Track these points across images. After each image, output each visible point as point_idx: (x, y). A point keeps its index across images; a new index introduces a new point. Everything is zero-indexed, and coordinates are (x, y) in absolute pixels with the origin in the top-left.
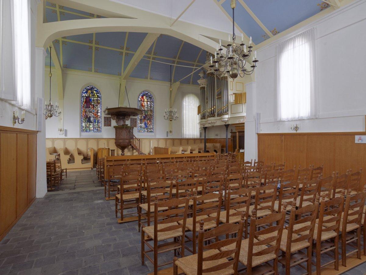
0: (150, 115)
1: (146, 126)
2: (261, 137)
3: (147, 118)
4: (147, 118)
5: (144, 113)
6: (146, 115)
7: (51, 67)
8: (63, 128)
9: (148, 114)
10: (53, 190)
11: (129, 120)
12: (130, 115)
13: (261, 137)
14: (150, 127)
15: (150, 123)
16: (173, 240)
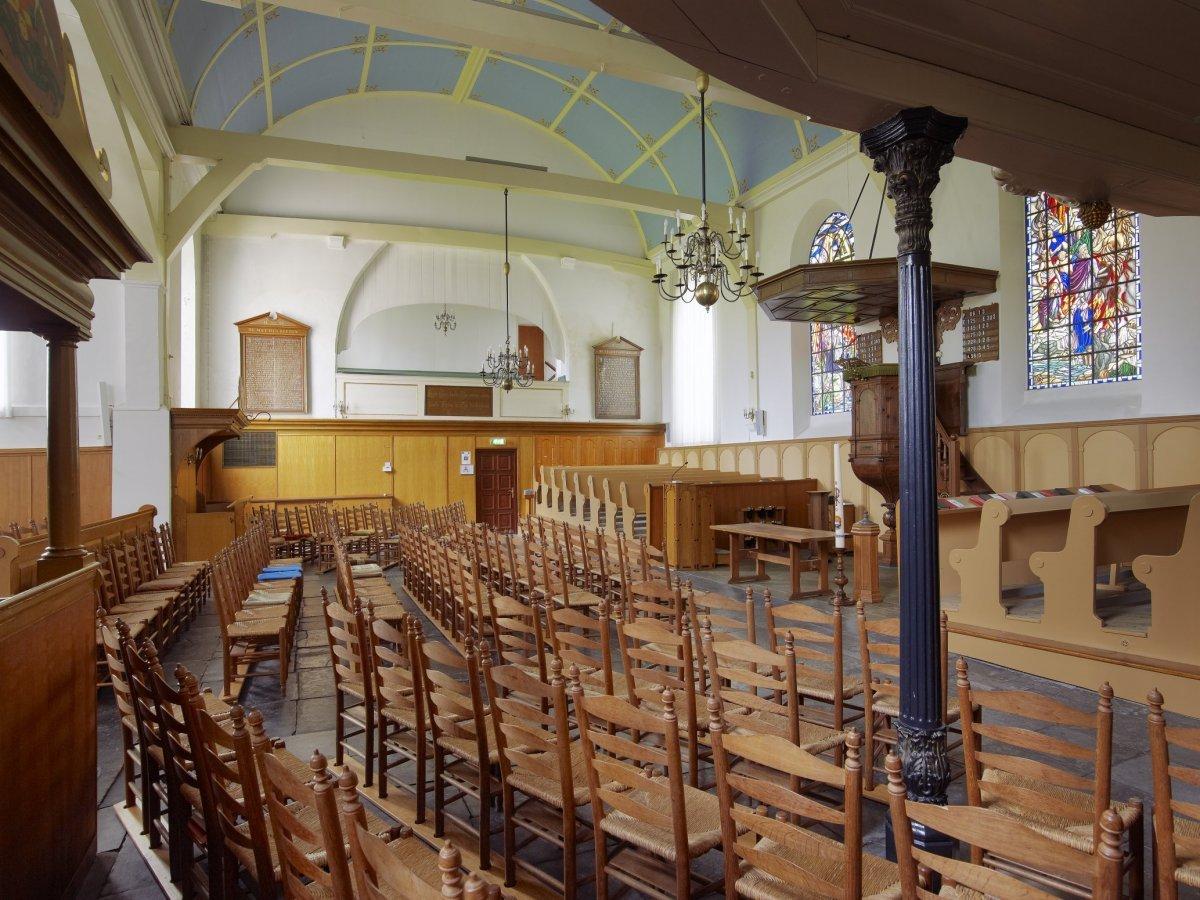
0: (1116, 251)
1: (1086, 340)
2: (426, 413)
3: (1087, 284)
4: (1087, 284)
5: (1068, 251)
6: (1079, 263)
7: (509, 237)
8: (756, 406)
9: (1097, 249)
10: (742, 578)
11: (960, 324)
12: (960, 295)
13: (426, 413)
14: (1113, 339)
15: (1110, 312)
16: (957, 886)
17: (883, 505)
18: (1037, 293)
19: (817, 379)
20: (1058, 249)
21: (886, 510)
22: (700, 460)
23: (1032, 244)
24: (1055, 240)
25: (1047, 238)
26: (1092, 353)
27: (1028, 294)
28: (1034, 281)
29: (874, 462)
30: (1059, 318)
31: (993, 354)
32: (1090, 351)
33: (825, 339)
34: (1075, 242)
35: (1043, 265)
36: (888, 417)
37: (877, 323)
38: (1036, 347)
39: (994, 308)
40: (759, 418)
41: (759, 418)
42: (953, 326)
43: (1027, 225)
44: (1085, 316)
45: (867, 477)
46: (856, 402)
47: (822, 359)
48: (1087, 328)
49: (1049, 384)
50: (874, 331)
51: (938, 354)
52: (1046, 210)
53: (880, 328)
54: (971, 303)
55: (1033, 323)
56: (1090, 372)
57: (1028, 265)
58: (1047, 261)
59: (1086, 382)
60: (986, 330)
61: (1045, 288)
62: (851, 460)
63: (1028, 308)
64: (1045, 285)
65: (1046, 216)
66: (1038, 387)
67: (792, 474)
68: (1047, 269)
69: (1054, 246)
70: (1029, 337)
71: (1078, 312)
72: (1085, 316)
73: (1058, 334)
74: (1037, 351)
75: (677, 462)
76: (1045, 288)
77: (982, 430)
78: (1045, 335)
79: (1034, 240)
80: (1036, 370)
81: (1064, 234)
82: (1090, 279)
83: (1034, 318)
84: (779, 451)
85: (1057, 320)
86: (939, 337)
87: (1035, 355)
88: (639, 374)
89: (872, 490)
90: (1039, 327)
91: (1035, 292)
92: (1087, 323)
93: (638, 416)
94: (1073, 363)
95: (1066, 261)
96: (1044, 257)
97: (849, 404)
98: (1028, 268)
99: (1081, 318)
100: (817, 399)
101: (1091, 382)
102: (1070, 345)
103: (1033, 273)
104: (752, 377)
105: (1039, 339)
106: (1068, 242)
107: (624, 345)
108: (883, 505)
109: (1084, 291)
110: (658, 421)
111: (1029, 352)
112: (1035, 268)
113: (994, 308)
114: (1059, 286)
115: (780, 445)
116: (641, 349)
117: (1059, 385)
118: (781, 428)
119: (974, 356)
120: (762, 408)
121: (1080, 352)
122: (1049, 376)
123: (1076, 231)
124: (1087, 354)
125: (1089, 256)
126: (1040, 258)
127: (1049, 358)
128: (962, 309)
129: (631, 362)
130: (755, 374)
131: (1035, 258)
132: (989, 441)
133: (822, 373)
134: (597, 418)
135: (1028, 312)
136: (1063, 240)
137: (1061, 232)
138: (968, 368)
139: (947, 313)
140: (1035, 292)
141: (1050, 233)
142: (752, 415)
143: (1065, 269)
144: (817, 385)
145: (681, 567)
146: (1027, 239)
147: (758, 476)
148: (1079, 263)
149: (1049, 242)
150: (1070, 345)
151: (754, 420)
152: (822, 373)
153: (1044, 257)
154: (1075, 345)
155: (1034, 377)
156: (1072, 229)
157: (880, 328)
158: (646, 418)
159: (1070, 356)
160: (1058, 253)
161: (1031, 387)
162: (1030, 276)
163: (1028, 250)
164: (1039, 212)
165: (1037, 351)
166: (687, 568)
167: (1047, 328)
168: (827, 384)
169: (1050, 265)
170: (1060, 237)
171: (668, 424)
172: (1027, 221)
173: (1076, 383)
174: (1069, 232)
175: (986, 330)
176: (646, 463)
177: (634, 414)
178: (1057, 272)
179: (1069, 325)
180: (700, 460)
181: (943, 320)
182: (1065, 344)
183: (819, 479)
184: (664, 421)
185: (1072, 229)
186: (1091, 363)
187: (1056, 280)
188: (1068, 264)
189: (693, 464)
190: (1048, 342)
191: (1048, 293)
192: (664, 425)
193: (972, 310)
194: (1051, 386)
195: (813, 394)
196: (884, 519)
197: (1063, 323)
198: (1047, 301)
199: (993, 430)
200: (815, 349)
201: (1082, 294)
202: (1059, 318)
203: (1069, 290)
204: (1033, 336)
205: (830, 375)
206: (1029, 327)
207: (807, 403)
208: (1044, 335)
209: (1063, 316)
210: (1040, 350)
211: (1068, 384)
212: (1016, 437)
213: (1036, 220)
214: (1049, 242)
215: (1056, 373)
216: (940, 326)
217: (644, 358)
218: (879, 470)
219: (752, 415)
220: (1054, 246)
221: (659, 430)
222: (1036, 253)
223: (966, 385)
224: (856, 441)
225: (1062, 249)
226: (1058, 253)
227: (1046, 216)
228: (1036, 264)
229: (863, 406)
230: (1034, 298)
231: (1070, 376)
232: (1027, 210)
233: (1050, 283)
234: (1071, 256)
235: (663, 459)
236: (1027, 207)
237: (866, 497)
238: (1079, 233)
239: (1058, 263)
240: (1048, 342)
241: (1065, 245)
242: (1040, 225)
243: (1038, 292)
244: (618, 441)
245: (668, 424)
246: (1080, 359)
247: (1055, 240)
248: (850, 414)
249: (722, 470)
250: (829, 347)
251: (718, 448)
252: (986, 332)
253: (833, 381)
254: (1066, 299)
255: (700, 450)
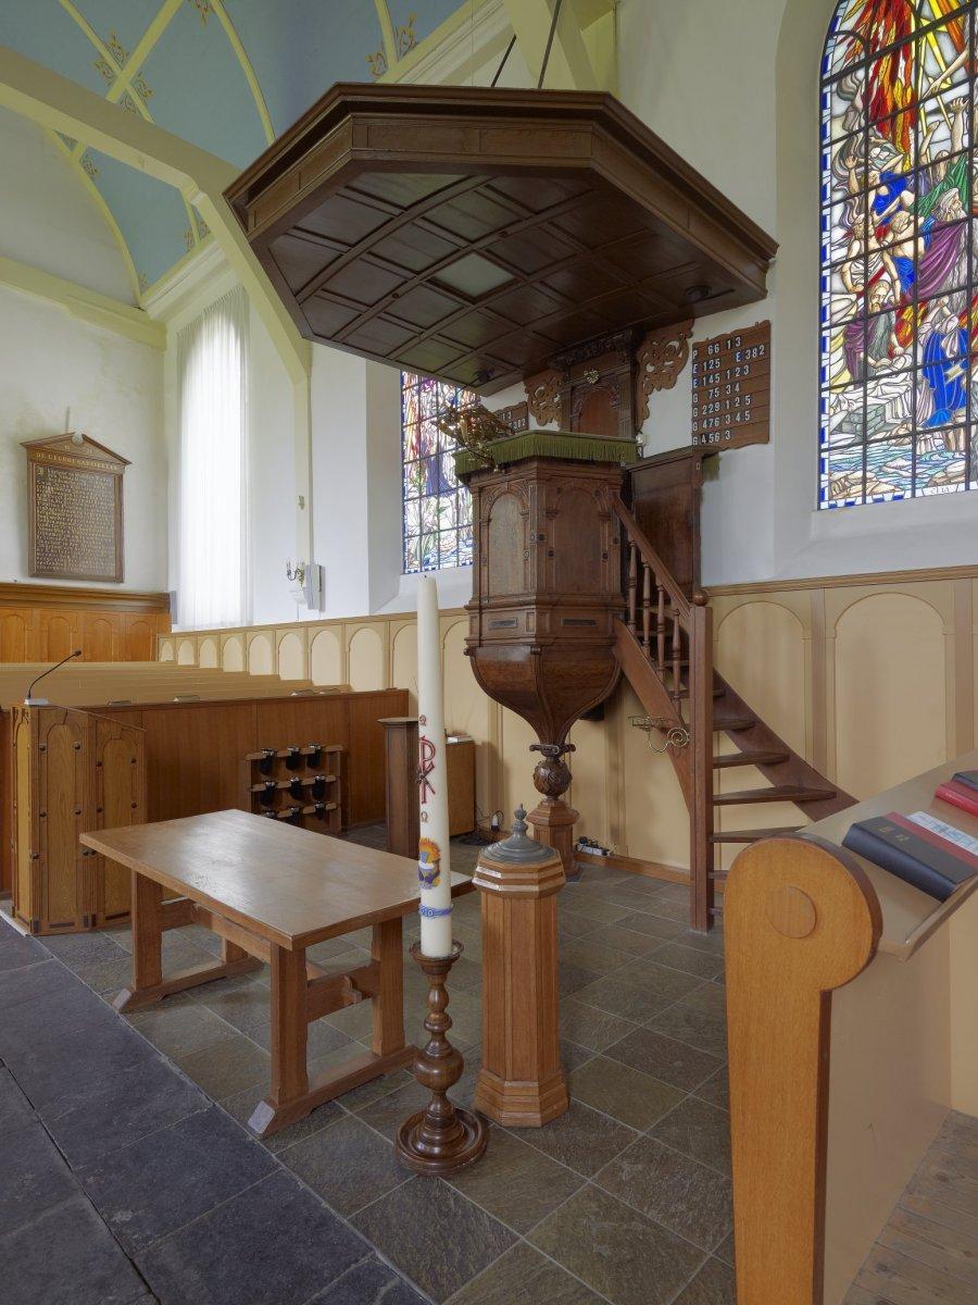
5: (915, 210)
11: (686, 378)
12: (685, 317)
17: (534, 748)
18: (841, 306)
19: (411, 508)
20: (892, 207)
21: (539, 757)
22: (197, 656)
23: (832, 205)
24: (884, 191)
25: (866, 188)
26: (967, 426)
27: (823, 311)
28: (835, 283)
29: (520, 654)
30: (891, 355)
31: (757, 430)
32: (962, 420)
33: (425, 436)
34: (930, 188)
35: (857, 247)
36: (551, 554)
37: (521, 386)
38: (837, 420)
39: (762, 332)
40: (312, 579)
41: (312, 579)
42: (669, 381)
43: (823, 166)
44: (950, 347)
45: (502, 688)
46: (482, 523)
47: (420, 473)
48: (955, 371)
49: (864, 496)
50: (514, 403)
51: (639, 439)
52: (865, 129)
53: (525, 397)
54: (709, 328)
55: (832, 371)
56: (960, 466)
57: (823, 250)
58: (866, 238)
59: (952, 488)
60: (743, 380)
61: (859, 295)
62: (470, 652)
63: (823, 341)
64: (860, 288)
65: (867, 140)
66: (841, 503)
67: (366, 679)
68: (865, 256)
69: (881, 203)
70: (822, 402)
71: (936, 338)
72: (950, 347)
73: (885, 388)
74: (839, 429)
75: (185, 658)
76: (859, 295)
77: (737, 590)
78: (859, 393)
79: (838, 196)
80: (836, 467)
81: (903, 176)
82: (964, 265)
83: (835, 361)
84: (344, 636)
85: (885, 361)
86: (640, 409)
87: (835, 438)
88: (121, 504)
89: (506, 710)
90: (846, 377)
91: (837, 307)
92: (956, 360)
93: (119, 579)
94: (921, 448)
95: (909, 232)
96: (860, 230)
97: (468, 552)
98: (823, 257)
99: (943, 352)
100: (412, 545)
101: (962, 487)
102: (914, 411)
103: (833, 265)
104: (302, 505)
105: (844, 402)
106: (915, 190)
107: (90, 450)
108: (534, 748)
109: (950, 293)
110: (161, 589)
111: (822, 432)
112: (838, 254)
113: (762, 332)
114: (892, 286)
115: (345, 627)
116: (126, 462)
117: (888, 497)
118: (348, 598)
119: (715, 438)
120: (318, 561)
121: (938, 422)
122: (864, 480)
123: (935, 163)
124: (956, 426)
125: (962, 214)
126: (850, 233)
127: (865, 442)
128: (691, 342)
129: (110, 482)
130: (307, 501)
131: (839, 233)
132: (752, 611)
133: (421, 497)
134: (33, 576)
135: (822, 348)
136: (904, 187)
137: (898, 170)
138: (703, 459)
139: (657, 358)
140: (837, 307)
141: (875, 175)
142: (302, 574)
143: (908, 250)
144: (412, 521)
145: (45, 927)
146: (823, 196)
147: (349, 687)
148: (938, 232)
149: (872, 196)
150: (914, 411)
151: (305, 585)
152: (421, 497)
153: (860, 230)
154: (927, 410)
155: (831, 483)
156: (924, 161)
157: (525, 397)
158: (134, 581)
159: (914, 435)
160: (891, 216)
161: (824, 505)
162: (826, 273)
163: (823, 220)
164: (851, 135)
165: (839, 429)
166: (64, 927)
167: (862, 377)
168: (429, 519)
169: (873, 244)
170: (896, 183)
171: (175, 593)
172: (823, 159)
173: (928, 491)
174: (918, 168)
175: (743, 380)
176: (135, 659)
177: (113, 574)
178: (887, 258)
179: (913, 369)
180: (197, 656)
181: (650, 369)
182: (902, 409)
183: (411, 690)
184: (171, 589)
185: (924, 161)
186: (962, 445)
187: (885, 276)
188: (914, 238)
189: (208, 661)
190: (865, 406)
191: (866, 303)
192: (168, 595)
193: (713, 342)
194: (869, 500)
195: (404, 535)
196: (536, 777)
197: (899, 366)
198: (860, 325)
199: (761, 589)
200: (410, 455)
201: (946, 300)
202: (891, 355)
203: (915, 296)
204: (830, 398)
205: (433, 500)
206: (822, 378)
207: (391, 549)
208: (855, 394)
209: (899, 350)
210: (846, 427)
211: (908, 494)
212: (814, 604)
213: (843, 154)
214: (872, 196)
215: (881, 471)
216: (644, 383)
217: (129, 476)
218: (530, 674)
219: (302, 574)
220: (881, 203)
221: (161, 604)
222: (841, 224)
223: (697, 496)
224: (481, 608)
225: (901, 207)
226: (891, 216)
227: (867, 140)
228: (841, 246)
229: (497, 529)
230: (836, 318)
231: (914, 476)
232: (823, 135)
233: (871, 283)
234: (921, 220)
235: (166, 654)
236: (823, 128)
237: (496, 726)
238: (942, 169)
239: (890, 238)
240: (865, 406)
241: (908, 197)
242: (851, 164)
243: (844, 304)
244: (74, 624)
245: (175, 593)
246: (937, 440)
247: (884, 191)
248: (470, 569)
249: (253, 672)
250: (433, 450)
251: (246, 632)
252: (741, 393)
253: (439, 510)
254: (908, 314)
255: (219, 635)
